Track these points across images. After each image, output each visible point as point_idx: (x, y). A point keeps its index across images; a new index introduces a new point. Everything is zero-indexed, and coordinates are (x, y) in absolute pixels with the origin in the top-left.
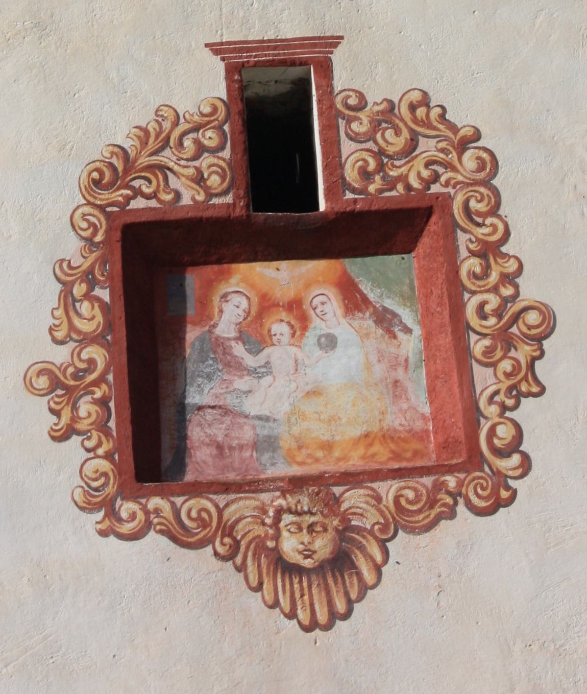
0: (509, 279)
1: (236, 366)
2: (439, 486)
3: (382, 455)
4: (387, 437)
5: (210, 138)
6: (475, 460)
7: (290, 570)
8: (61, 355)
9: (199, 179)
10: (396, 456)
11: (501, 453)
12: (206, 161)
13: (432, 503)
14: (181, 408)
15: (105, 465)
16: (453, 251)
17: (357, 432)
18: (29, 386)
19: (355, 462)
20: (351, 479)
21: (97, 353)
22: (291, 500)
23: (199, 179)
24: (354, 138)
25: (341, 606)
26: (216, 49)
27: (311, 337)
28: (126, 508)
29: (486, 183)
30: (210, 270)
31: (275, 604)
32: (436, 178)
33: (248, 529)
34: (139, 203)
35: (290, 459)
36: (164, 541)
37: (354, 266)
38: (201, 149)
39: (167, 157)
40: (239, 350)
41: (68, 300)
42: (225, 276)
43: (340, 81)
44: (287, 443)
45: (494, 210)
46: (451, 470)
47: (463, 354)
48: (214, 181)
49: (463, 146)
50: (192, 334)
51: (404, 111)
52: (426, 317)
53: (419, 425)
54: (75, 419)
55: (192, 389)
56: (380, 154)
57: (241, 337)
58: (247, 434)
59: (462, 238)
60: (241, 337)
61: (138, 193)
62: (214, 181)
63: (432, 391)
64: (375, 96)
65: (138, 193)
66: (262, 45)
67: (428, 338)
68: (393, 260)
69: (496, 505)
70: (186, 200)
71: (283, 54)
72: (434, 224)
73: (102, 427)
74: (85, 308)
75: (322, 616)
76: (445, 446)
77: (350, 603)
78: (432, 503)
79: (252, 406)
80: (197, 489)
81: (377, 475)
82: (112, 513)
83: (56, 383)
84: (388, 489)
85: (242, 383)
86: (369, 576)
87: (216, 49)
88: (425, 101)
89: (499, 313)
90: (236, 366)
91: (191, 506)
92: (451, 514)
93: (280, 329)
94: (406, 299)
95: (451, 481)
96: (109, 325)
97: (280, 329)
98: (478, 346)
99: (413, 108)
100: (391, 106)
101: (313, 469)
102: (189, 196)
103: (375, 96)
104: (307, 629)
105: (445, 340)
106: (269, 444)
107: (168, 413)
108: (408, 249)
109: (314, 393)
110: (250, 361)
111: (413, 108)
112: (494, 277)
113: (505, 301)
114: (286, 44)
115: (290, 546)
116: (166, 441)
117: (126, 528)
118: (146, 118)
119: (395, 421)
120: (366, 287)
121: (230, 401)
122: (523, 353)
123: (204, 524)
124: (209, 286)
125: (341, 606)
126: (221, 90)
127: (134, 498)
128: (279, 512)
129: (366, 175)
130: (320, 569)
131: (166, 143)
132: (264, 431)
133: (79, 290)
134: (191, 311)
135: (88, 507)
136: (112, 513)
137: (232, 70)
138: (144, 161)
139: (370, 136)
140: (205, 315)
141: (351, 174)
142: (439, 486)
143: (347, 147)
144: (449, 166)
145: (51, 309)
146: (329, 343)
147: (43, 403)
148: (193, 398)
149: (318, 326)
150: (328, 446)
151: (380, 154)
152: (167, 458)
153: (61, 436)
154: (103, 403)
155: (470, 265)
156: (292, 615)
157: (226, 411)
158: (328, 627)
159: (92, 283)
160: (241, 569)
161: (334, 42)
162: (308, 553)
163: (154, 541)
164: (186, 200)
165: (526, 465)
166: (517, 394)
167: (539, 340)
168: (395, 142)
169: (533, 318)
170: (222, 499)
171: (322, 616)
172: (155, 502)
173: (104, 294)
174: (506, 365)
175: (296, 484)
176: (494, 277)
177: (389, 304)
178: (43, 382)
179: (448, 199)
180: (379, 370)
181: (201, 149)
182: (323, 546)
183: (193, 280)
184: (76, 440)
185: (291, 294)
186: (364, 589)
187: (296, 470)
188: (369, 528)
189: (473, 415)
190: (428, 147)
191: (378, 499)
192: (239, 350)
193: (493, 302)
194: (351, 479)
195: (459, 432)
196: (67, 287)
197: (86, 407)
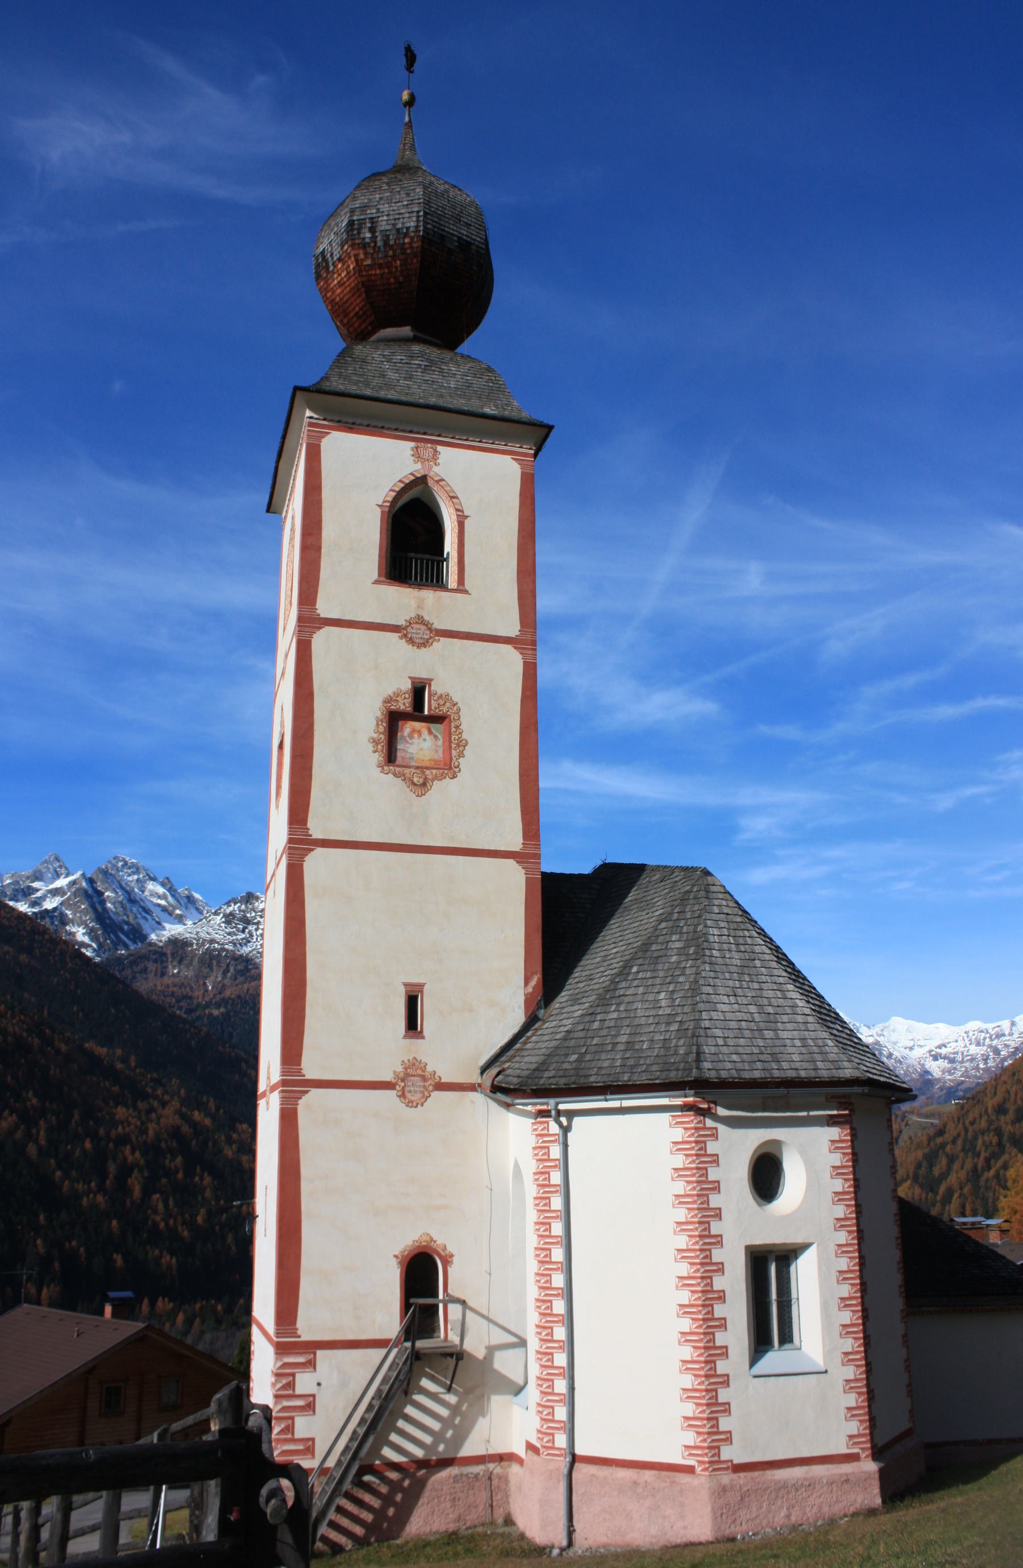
0: (460, 733)
1: (407, 742)
2: (443, 772)
3: (432, 764)
4: (434, 760)
5: (407, 696)
6: (450, 768)
7: (415, 784)
8: (375, 736)
9: (404, 704)
10: (435, 764)
11: (456, 767)
12: (406, 701)
13: (442, 775)
14: (396, 749)
15: (382, 759)
16: (450, 726)
17: (428, 758)
18: (369, 741)
19: (428, 764)
20: (427, 768)
21: (382, 736)
22: (416, 771)
23: (404, 704)
24: (434, 700)
25: (424, 793)
26: (410, 678)
27: (421, 738)
28: (386, 768)
29: (458, 713)
30: (403, 722)
31: (412, 791)
32: (448, 711)
33: (408, 775)
34: (392, 707)
35: (416, 762)
36: (392, 776)
37: (431, 726)
38: (405, 698)
39: (398, 699)
40: (408, 739)
41: (378, 725)
42: (406, 723)
43: (432, 688)
44: (415, 759)
45: (459, 719)
46: (446, 769)
47: (450, 747)
48: (407, 705)
49: (454, 705)
50: (399, 734)
51: (444, 696)
52: (443, 738)
53: (440, 759)
54: (377, 748)
55: (163, 939)
56: (439, 704)
57: (409, 736)
58: (408, 756)
59: (452, 724)
60: (409, 736)
61: (392, 705)
62: (407, 705)
63: (443, 752)
64: (439, 693)
65: (392, 705)
66: (419, 678)
67: (443, 742)
68: (438, 725)
69: (454, 777)
70: (401, 708)
71: (422, 681)
72: (447, 720)
73: (382, 751)
74: (381, 727)
75: (420, 794)
76: (445, 764)
77: (425, 792)
78: (442, 775)
79: (410, 750)
80: (398, 766)
81: (433, 768)
82: (383, 769)
83: (374, 741)
84: (434, 771)
85: (408, 746)
86: (429, 788)
87: (410, 678)
88: (448, 695)
89: (458, 740)
90: (407, 742)
91: (398, 769)
92: (445, 778)
93: (416, 736)
94: (440, 734)
95: (446, 772)
96: (385, 731)
97: (416, 736)
98: (453, 746)
99: (446, 696)
100: (442, 695)
101: (419, 765)
102: (402, 707)
103: (439, 693)
104: (418, 796)
105: (447, 743)
106: (412, 758)
107: (394, 749)
108: (441, 723)
109: (421, 750)
110: (410, 741)
111: (446, 696)
112: (457, 733)
113: (459, 738)
114: (423, 679)
115: (415, 780)
116: (393, 755)
117: (386, 772)
118: (395, 690)
119: (436, 757)
120: (434, 731)
121: (405, 749)
122: (461, 748)
123: (400, 773)
124: (403, 725)
125: (424, 793)
126: (410, 687)
127: (386, 766)
128: (414, 773)
129: (436, 708)
130: (420, 785)
131: (398, 696)
132: (411, 755)
133: (380, 723)
134: (399, 729)
135: (379, 767)
136: (383, 769)
137: (413, 683)
138: (394, 698)
139: (437, 701)
140: (402, 731)
141: (433, 708)
142: (443, 772)
143: (433, 702)
144: (451, 709)
145: (465, 763)
146: (425, 740)
147: (372, 745)
148: (399, 747)
149: (423, 736)
150: (423, 761)
151: (439, 704)
152: (393, 758)
153: (375, 752)
154: (383, 746)
155: (453, 729)
156: (414, 793)
157: (404, 751)
158: (421, 796)
159: (382, 722)
160: (406, 783)
161: (431, 680)
162: (418, 782)
163: (390, 776)
164: (401, 708)
165: (460, 771)
166: (460, 756)
167: (465, 746)
168: (441, 702)
169: (464, 742)
170: (403, 769)
171: (420, 794)
172: (391, 768)
173: (385, 725)
174: (458, 751)
175: (417, 768)
176: (457, 733)
177: (437, 734)
178: (372, 741)
179: (450, 715)
180: (434, 747)
181: (405, 698)
182: (421, 781)
183: (400, 723)
184: (377, 753)
185: (418, 729)
186: (428, 790)
187: (417, 764)
188: (899, 1550)
189: (451, 759)
190: (448, 705)
191: (432, 773)
192: (408, 739)
193: (457, 738)
194: (427, 768)
195: (448, 762)
196: (378, 722)
197: (380, 747)
